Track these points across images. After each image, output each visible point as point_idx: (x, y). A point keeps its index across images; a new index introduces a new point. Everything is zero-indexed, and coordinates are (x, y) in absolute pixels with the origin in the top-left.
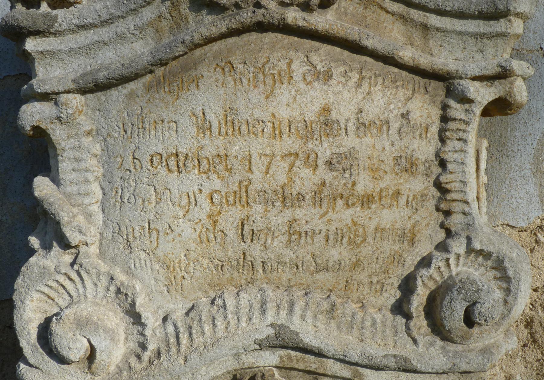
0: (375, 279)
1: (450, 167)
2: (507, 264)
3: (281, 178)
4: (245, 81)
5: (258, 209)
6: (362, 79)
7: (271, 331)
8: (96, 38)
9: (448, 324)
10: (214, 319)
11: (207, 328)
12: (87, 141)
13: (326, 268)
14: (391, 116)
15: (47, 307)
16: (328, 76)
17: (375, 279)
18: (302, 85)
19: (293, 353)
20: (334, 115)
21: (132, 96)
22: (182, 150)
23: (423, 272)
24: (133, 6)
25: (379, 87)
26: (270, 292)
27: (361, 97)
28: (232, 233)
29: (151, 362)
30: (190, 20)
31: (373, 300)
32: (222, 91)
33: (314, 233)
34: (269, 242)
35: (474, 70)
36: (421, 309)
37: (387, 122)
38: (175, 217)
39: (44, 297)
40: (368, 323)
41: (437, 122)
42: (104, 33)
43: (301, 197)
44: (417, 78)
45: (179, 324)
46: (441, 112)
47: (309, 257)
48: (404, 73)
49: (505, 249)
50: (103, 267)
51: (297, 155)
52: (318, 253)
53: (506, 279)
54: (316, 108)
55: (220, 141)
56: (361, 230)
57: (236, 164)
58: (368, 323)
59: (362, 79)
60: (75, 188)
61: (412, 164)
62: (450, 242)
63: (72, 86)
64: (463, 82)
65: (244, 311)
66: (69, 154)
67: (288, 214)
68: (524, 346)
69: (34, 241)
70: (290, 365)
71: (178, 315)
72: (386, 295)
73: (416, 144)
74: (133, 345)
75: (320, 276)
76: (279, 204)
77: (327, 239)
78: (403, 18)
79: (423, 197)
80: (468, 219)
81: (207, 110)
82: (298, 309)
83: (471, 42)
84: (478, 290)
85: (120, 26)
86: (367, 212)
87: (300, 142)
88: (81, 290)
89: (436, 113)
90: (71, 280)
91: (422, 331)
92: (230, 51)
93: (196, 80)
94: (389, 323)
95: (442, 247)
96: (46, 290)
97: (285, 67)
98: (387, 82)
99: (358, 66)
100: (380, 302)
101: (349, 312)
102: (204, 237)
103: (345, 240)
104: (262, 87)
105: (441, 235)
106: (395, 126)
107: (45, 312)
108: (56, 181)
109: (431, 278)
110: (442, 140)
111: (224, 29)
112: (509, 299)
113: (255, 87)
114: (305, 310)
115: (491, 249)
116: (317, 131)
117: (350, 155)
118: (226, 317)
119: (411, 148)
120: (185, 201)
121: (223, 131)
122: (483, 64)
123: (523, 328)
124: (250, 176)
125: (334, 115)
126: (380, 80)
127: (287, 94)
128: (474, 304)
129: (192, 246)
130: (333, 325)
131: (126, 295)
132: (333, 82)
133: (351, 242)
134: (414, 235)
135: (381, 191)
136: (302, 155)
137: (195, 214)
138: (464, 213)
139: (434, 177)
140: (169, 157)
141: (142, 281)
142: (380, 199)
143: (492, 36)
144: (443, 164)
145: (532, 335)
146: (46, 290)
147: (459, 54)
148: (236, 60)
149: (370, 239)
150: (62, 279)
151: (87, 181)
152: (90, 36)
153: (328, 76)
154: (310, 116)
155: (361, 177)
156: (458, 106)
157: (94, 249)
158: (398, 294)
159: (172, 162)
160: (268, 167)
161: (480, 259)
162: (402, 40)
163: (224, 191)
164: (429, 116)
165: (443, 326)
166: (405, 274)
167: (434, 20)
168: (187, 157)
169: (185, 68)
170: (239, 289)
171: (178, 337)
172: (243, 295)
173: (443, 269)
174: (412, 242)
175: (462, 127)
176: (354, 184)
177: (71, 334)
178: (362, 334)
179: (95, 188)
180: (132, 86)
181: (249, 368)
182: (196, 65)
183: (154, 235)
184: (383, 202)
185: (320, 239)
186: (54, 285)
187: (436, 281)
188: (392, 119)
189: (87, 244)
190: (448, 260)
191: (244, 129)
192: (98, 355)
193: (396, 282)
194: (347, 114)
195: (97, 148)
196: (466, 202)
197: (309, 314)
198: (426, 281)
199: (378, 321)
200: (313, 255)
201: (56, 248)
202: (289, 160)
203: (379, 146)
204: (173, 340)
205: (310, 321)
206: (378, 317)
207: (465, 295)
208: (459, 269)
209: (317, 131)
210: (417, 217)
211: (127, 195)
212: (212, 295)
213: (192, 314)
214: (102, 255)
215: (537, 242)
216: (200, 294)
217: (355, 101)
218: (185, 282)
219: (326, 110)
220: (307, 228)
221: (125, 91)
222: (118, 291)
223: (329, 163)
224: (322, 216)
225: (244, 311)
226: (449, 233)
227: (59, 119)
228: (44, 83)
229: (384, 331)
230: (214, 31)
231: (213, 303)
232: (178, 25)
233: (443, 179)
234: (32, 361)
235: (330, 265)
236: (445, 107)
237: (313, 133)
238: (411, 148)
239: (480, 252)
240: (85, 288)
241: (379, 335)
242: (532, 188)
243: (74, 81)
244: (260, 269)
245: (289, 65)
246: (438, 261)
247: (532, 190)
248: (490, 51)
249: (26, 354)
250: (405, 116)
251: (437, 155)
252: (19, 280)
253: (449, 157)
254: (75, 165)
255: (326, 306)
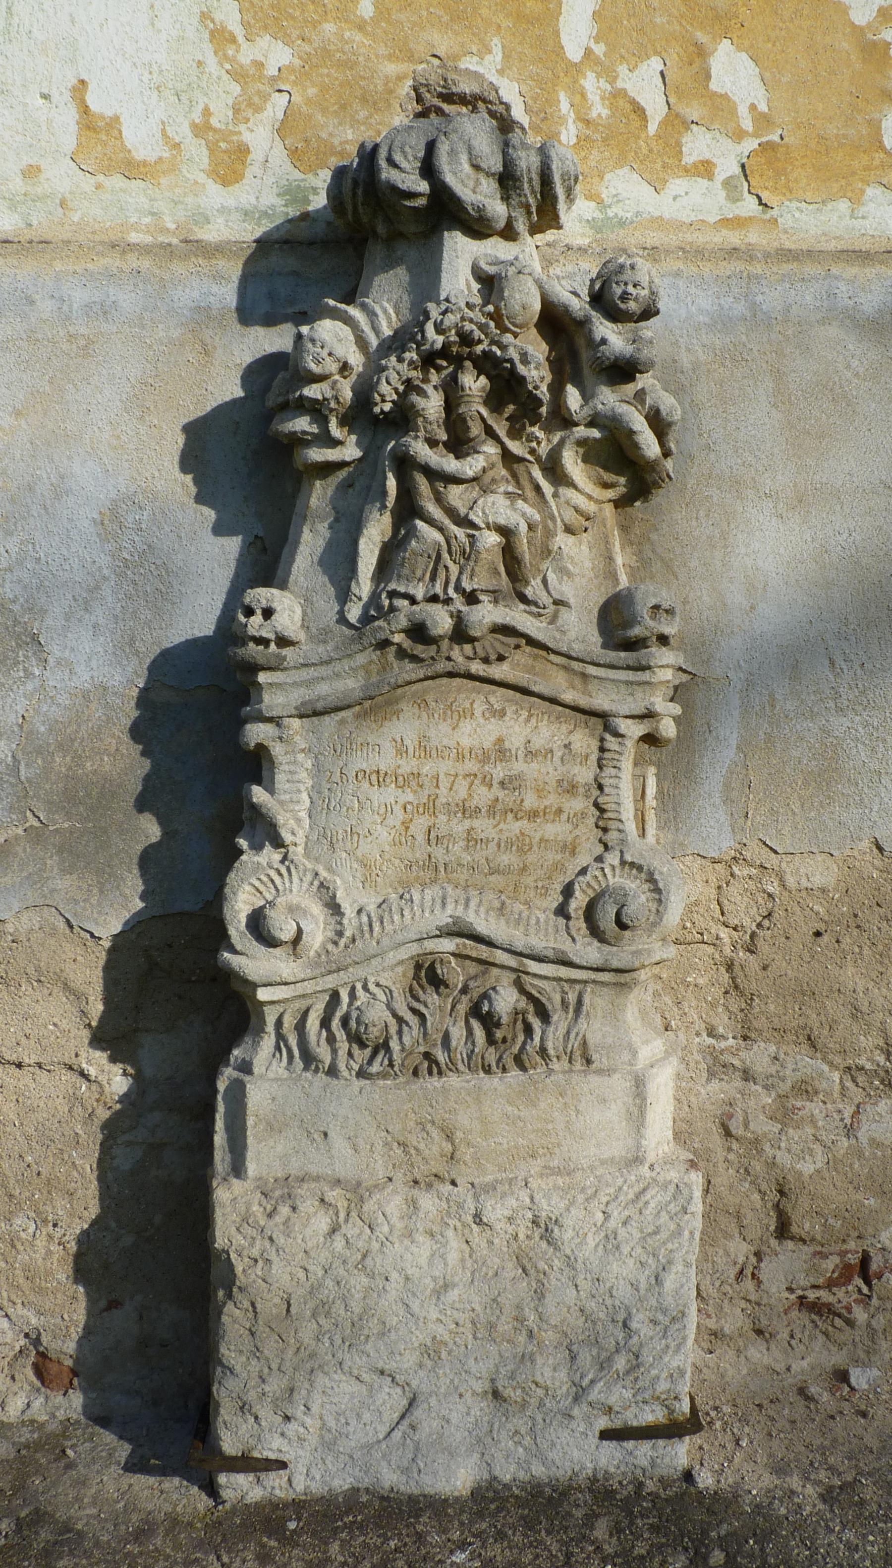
0: (540, 884)
1: (606, 790)
2: (657, 876)
3: (463, 793)
4: (436, 716)
5: (443, 818)
6: (530, 716)
7: (450, 920)
8: (316, 674)
9: (602, 925)
10: (402, 910)
11: (396, 918)
12: (301, 757)
13: (498, 872)
14: (555, 747)
15: (255, 899)
16: (502, 714)
17: (540, 884)
18: (481, 720)
19: (467, 942)
20: (507, 745)
21: (343, 722)
22: (383, 769)
23: (581, 878)
24: (349, 652)
25: (545, 722)
26: (450, 890)
27: (529, 730)
28: (421, 838)
29: (346, 947)
30: (395, 666)
31: (538, 903)
32: (417, 723)
33: (488, 840)
34: (450, 846)
35: (625, 710)
36: (581, 912)
37: (552, 751)
38: (375, 823)
39: (253, 891)
40: (533, 921)
41: (596, 752)
42: (323, 671)
43: (477, 810)
44: (578, 715)
45: (373, 915)
46: (599, 744)
47: (483, 861)
48: (567, 710)
49: (656, 863)
50: (309, 866)
51: (475, 775)
52: (491, 858)
53: (658, 890)
54: (493, 738)
55: (414, 762)
56: (527, 840)
57: (426, 781)
58: (533, 921)
59: (530, 716)
60: (288, 797)
61: (573, 786)
62: (606, 855)
63: (294, 712)
64: (616, 720)
65: (428, 904)
66: (286, 768)
67: (467, 824)
68: (726, 993)
69: (243, 843)
70: (465, 952)
71: (372, 908)
72: (550, 899)
73: (576, 770)
74: (330, 934)
75: (492, 878)
76: (459, 815)
77: (499, 846)
78: (566, 668)
79: (584, 815)
80: (621, 836)
81: (405, 737)
82: (473, 905)
83: (623, 687)
84: (625, 895)
85: (338, 667)
86: (533, 825)
87: (478, 765)
88: (287, 885)
89: (595, 744)
90: (280, 874)
91: (582, 932)
92: (425, 691)
93: (397, 713)
94: (551, 923)
95: (599, 859)
96: (257, 883)
97: (468, 706)
98: (552, 719)
99: (528, 705)
100: (545, 905)
101: (516, 910)
102: (397, 841)
103: (514, 848)
104: (449, 720)
105: (600, 849)
106: (558, 754)
107: (253, 905)
108: (271, 790)
109: (588, 885)
110: (601, 767)
111: (422, 676)
112: (661, 909)
113: (444, 720)
114: (479, 906)
115: (642, 862)
116: (493, 757)
117: (519, 777)
118: (412, 909)
119: (572, 773)
120: (383, 810)
121: (417, 754)
122: (633, 706)
123: (724, 972)
124: (438, 791)
125: (507, 745)
126: (546, 717)
127: (469, 727)
128: (623, 906)
129: (387, 848)
130: (503, 921)
131: (328, 888)
132: (507, 718)
133: (519, 849)
134: (574, 848)
135: (546, 807)
136: (479, 776)
137: (390, 821)
138: (619, 831)
139: (593, 798)
140: (371, 773)
141: (342, 878)
142: (545, 814)
143: (640, 684)
144: (600, 787)
145: (733, 979)
146: (257, 883)
147: (614, 696)
148: (430, 698)
149: (535, 848)
150: (273, 874)
151: (299, 791)
152: (312, 672)
153: (502, 714)
154: (487, 745)
155: (529, 795)
156: (613, 739)
157: (300, 849)
158: (561, 899)
159: (374, 778)
160: (452, 785)
161: (634, 871)
162: (565, 685)
163: (416, 802)
164: (589, 746)
165: (598, 927)
166: (567, 881)
167: (592, 670)
168: (386, 774)
169: (389, 703)
170: (424, 885)
171: (371, 926)
172: (427, 891)
173: (600, 878)
174: (573, 853)
175: (616, 757)
176: (522, 801)
177: (283, 917)
178: (527, 930)
179: (305, 796)
180: (343, 714)
181: (431, 954)
182: (397, 702)
183: (355, 837)
184: (547, 817)
185: (493, 846)
186: (265, 879)
187: (594, 890)
188: (555, 749)
189: (296, 845)
190: (602, 869)
191: (434, 753)
192: (304, 936)
193: (559, 888)
194: (516, 744)
195: (309, 764)
196: (620, 821)
197: (482, 909)
198: (584, 887)
199: (542, 920)
200: (487, 859)
201: (268, 848)
202: (469, 780)
203: (543, 770)
204: (366, 928)
205: (483, 916)
206: (542, 917)
207: (615, 898)
208: (616, 880)
209: (493, 757)
210: (577, 832)
211: (333, 804)
212: (401, 891)
213: (384, 906)
214: (307, 854)
215: (732, 875)
216: (390, 890)
217: (524, 733)
218: (378, 879)
219: (500, 740)
220: (482, 836)
221: (337, 718)
222: (322, 885)
223: (502, 783)
224: (495, 826)
225: (428, 904)
226: (606, 847)
227: (280, 738)
228: (270, 707)
229: (547, 929)
230: (414, 677)
231: (401, 897)
232: (384, 669)
233: (600, 800)
234: (239, 947)
235: (501, 869)
236: (602, 740)
237: (489, 758)
238: (572, 773)
239: (632, 865)
240: (291, 882)
241: (543, 932)
242: (722, 815)
243: (296, 708)
244: (442, 870)
245: (472, 704)
246: (594, 871)
247: (722, 819)
248: (639, 695)
249: (233, 941)
250: (567, 746)
251: (596, 780)
252: (232, 875)
253: (606, 782)
254: (289, 776)
255: (497, 904)
